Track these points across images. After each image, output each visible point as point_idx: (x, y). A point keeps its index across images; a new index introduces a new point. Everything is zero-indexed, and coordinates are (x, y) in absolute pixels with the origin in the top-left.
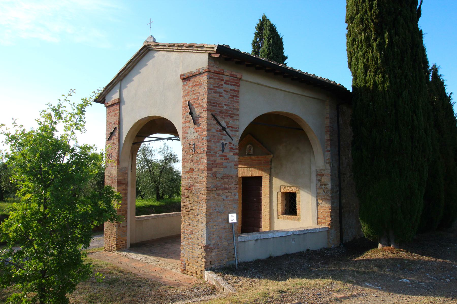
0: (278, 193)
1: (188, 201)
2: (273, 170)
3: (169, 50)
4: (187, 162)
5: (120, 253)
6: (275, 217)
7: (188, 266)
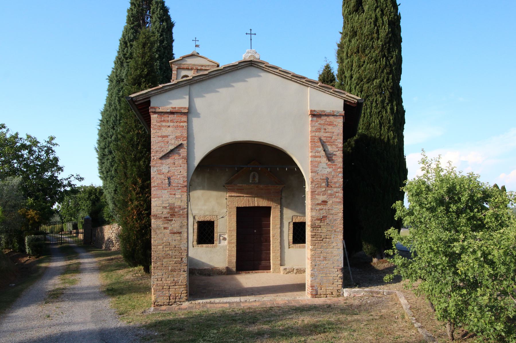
0: (289, 223)
1: (320, 231)
2: (283, 200)
3: (296, 81)
6: (285, 247)
7: (321, 289)
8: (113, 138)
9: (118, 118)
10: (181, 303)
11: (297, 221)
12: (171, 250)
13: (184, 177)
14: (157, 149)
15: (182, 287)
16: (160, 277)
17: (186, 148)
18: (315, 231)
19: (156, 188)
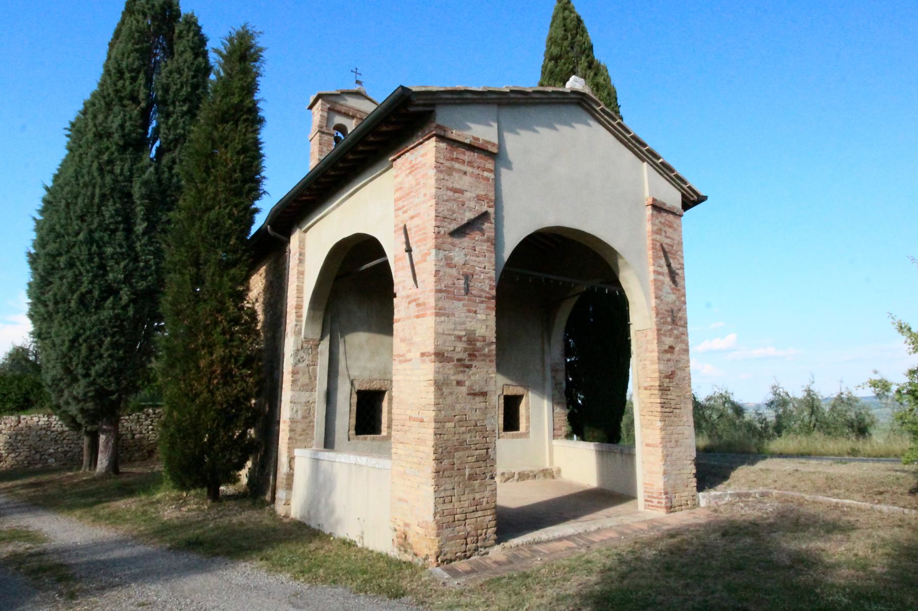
4: (665, 335)
5: (507, 544)
8: (81, 237)
9: (96, 200)
10: (487, 549)
11: (509, 393)
12: (470, 431)
13: (490, 279)
14: (446, 213)
15: (489, 512)
16: (449, 493)
17: (493, 221)
18: (664, 397)
19: (444, 294)
